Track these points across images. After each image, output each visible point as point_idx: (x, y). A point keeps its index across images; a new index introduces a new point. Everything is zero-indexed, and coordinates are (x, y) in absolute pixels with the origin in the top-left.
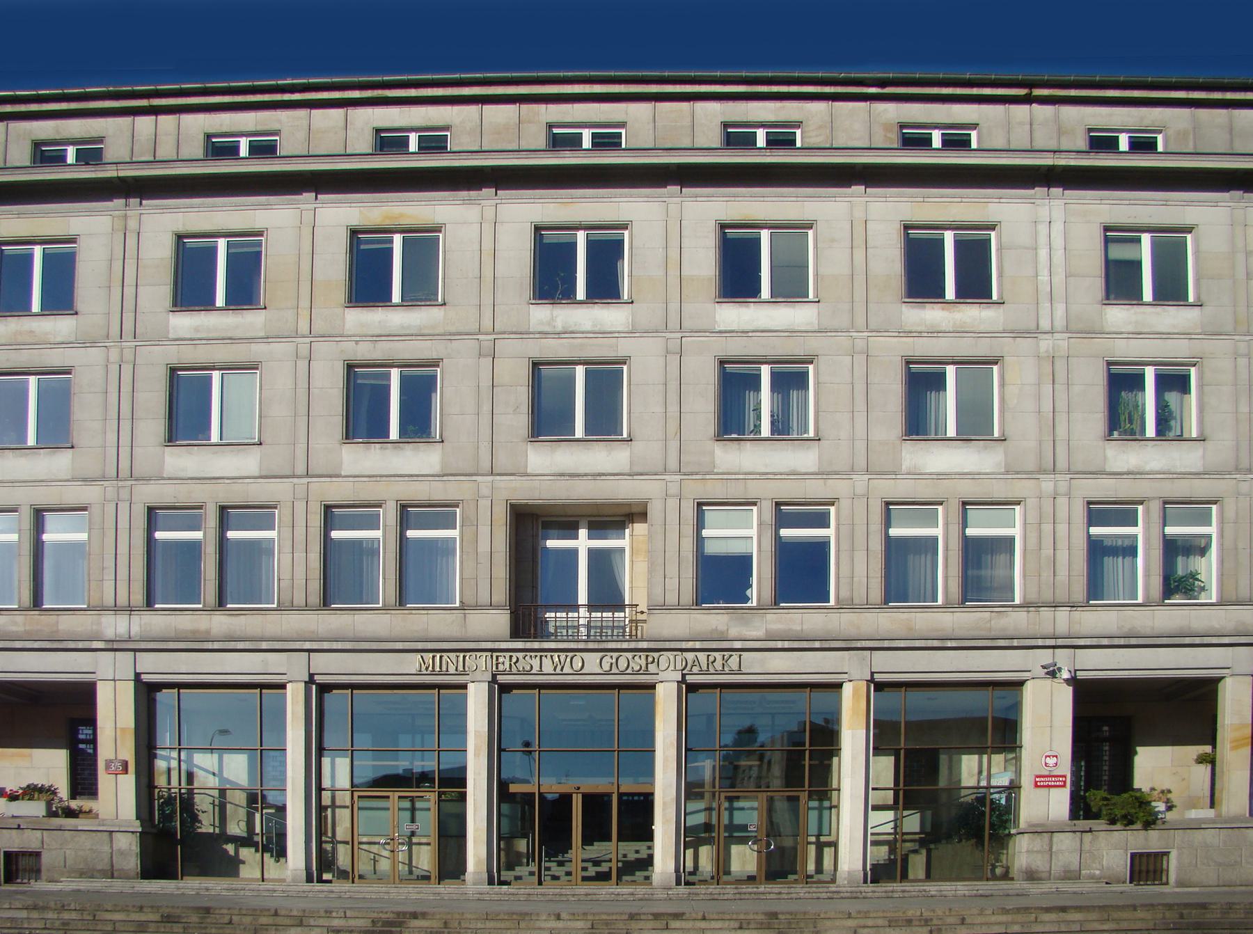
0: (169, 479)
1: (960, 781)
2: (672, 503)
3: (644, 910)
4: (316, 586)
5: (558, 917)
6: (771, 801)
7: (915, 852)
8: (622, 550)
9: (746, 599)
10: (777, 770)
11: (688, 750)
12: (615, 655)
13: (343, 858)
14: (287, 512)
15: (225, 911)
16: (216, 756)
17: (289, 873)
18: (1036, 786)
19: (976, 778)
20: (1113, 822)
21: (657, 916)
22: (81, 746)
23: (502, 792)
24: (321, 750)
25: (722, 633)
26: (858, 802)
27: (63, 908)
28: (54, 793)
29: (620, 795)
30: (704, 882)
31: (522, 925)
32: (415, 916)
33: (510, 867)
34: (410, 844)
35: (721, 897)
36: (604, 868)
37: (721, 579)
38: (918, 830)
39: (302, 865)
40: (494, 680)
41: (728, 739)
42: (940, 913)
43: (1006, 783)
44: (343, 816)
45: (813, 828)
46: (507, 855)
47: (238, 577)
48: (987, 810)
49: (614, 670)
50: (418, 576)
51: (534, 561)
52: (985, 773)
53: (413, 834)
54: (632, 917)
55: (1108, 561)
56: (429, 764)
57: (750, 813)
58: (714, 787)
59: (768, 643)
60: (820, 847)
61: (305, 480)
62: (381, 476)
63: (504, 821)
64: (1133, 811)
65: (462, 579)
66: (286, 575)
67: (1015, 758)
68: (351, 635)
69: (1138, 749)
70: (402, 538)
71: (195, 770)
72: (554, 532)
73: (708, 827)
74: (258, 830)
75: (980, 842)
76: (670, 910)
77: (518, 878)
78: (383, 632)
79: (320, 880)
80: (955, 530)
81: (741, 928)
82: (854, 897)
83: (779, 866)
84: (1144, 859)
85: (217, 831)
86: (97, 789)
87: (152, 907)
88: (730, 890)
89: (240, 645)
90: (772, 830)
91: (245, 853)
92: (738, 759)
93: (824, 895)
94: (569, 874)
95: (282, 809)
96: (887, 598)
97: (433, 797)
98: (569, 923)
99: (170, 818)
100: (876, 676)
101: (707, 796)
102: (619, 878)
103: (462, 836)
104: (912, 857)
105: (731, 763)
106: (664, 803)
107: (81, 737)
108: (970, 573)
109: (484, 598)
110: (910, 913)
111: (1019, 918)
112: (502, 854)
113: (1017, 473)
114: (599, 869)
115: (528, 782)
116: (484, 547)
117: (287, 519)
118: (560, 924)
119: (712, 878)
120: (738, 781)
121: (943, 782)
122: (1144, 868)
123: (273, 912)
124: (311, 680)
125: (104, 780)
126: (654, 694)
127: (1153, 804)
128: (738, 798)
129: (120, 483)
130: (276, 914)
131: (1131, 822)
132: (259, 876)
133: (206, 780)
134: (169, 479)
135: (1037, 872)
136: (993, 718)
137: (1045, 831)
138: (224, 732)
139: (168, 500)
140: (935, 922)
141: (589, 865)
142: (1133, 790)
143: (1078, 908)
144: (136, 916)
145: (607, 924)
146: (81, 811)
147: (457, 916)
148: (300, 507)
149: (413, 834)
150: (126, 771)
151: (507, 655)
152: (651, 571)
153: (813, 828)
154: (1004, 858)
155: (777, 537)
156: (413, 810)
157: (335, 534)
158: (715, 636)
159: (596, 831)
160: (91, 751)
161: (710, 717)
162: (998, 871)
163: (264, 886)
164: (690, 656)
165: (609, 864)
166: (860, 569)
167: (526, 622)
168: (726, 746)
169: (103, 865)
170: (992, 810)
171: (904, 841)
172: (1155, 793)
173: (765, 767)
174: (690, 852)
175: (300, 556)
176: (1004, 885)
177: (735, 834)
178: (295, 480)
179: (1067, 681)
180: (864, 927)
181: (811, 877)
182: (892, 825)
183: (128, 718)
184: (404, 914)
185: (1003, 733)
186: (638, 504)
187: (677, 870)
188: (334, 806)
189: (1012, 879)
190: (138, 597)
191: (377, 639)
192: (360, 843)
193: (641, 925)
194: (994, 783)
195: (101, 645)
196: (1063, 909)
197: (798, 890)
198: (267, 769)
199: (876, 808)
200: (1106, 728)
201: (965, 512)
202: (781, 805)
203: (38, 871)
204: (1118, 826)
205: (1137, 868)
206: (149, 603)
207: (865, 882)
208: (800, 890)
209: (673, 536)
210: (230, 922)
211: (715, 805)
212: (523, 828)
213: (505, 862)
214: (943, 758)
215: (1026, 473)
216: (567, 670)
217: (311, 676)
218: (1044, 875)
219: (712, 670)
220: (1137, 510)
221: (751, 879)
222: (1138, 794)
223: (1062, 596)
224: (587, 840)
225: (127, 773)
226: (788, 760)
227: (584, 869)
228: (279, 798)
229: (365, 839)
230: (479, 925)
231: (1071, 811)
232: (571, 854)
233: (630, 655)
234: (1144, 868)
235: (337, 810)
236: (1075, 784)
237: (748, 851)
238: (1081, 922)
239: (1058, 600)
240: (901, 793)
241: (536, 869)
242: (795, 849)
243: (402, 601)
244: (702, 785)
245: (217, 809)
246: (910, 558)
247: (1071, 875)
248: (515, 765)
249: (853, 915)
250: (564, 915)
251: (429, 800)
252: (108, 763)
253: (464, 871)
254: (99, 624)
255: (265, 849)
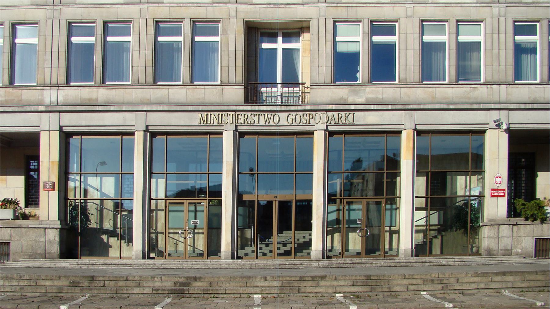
0: (79, 4)
1: (456, 192)
2: (322, 21)
3: (308, 274)
4: (150, 70)
5: (266, 279)
6: (368, 204)
7: (436, 237)
8: (298, 50)
9: (356, 79)
10: (371, 186)
11: (329, 173)
12: (295, 114)
13: (160, 245)
14: (137, 25)
15: (101, 278)
16: (99, 178)
17: (134, 253)
18: (492, 196)
19: (464, 190)
20: (527, 219)
21: (313, 278)
22: (32, 173)
23: (240, 201)
24: (151, 173)
25: (345, 100)
26: (409, 214)
27: (21, 278)
28: (18, 204)
29: (297, 201)
30: (336, 256)
31: (248, 285)
32: (195, 279)
33: (243, 248)
34: (194, 233)
35: (344, 266)
36: (288, 248)
37: (344, 66)
38: (437, 223)
39: (140, 248)
40: (236, 130)
41: (348, 166)
42: (447, 276)
43: (478, 194)
44: (161, 214)
45: (388, 223)
46: (241, 240)
47: (112, 65)
48: (469, 210)
49: (294, 124)
50: (200, 68)
51: (256, 56)
52: (468, 188)
53: (195, 227)
54: (302, 278)
55: (524, 56)
56: (203, 183)
57: (358, 213)
58: (341, 196)
59: (368, 106)
60: (392, 233)
61: (146, 6)
62: (183, 4)
63: (240, 218)
64: (536, 212)
65: (221, 67)
66: (135, 69)
67: (481, 178)
68: (166, 101)
69: (539, 173)
70: (193, 41)
71: (88, 188)
72: (265, 39)
73: (338, 221)
74: (119, 226)
75: (466, 232)
76: (319, 274)
77: (246, 254)
78: (182, 100)
79: (150, 258)
80: (453, 36)
81: (353, 285)
82: (407, 265)
83: (372, 247)
84: (541, 242)
85: (98, 227)
86: (39, 201)
87: (65, 276)
88: (348, 261)
89: (113, 108)
90: (369, 224)
91: (113, 241)
92: (352, 179)
93: (393, 265)
94: (271, 252)
95: (131, 212)
96: (422, 79)
97: (205, 203)
98: (271, 283)
99: (74, 219)
100: (417, 126)
101: (338, 201)
102: (295, 254)
103: (219, 228)
104: (434, 240)
105: (349, 181)
106: (317, 206)
107: (32, 167)
108: (460, 63)
109: (232, 80)
110: (433, 276)
111: (484, 279)
112: (239, 239)
113: (482, 3)
114: (286, 248)
115: (251, 193)
116: (232, 48)
117: (137, 30)
118: (266, 284)
119: (340, 254)
120: (353, 192)
121: (448, 194)
122: (541, 248)
123: (125, 278)
124: (147, 130)
125: (43, 195)
126: (313, 138)
127: (545, 208)
128: (352, 203)
129: (55, 7)
130: (127, 280)
131: (535, 220)
132: (119, 256)
133: (94, 194)
134: (79, 4)
135: (492, 250)
136: (472, 153)
137: (495, 224)
138: (103, 163)
139: (78, 18)
140: (445, 281)
141: (281, 246)
142: (536, 199)
143: (511, 273)
144: (57, 283)
145: (289, 283)
146: (30, 216)
147: (216, 279)
148: (143, 21)
149: (195, 227)
150: (53, 189)
151: (243, 113)
152: (312, 62)
153: (388, 223)
154: (477, 241)
155: (371, 41)
156: (196, 211)
157: (161, 39)
158: (342, 102)
159: (284, 226)
160: (36, 177)
161: (339, 151)
162: (474, 249)
163: (123, 262)
164: (330, 114)
165: (290, 245)
166: (410, 60)
167: (252, 95)
168: (347, 170)
169: (40, 251)
170: (471, 211)
171: (430, 230)
172: (546, 201)
173: (365, 182)
174: (329, 237)
175: (142, 52)
176: (476, 258)
177: (351, 226)
178: (141, 6)
179: (505, 130)
180: (412, 284)
181: (386, 253)
182: (425, 220)
183: (55, 156)
184: (190, 278)
185: (475, 163)
186: (305, 21)
187: (323, 249)
188: (157, 210)
189: (480, 255)
190: (62, 79)
191: (181, 104)
192: (169, 233)
193: (306, 283)
194: (472, 194)
195: (42, 109)
196: (504, 274)
197: (380, 261)
198: (124, 186)
199: (418, 209)
200: (523, 160)
201: (458, 25)
202: (373, 207)
203: (8, 255)
204: (529, 222)
205: (538, 248)
206: (68, 82)
207: (412, 256)
208: (382, 261)
209: (322, 41)
210: (104, 286)
211: (341, 207)
212: (249, 223)
213: (241, 243)
214: (449, 178)
215: (486, 3)
216: (272, 123)
217: (147, 127)
218: (495, 252)
219: (340, 123)
220: (536, 26)
221: (358, 254)
222: (538, 202)
223: (503, 79)
224: (280, 231)
225: (54, 190)
226: (376, 179)
227: (279, 249)
228: (130, 205)
229: (171, 231)
230: (227, 285)
231: (508, 212)
232: (272, 239)
233: (301, 114)
234: (541, 248)
235: (159, 212)
236: (509, 195)
237: (357, 236)
238: (512, 282)
239: (501, 80)
240: (429, 199)
241: (255, 249)
242: (379, 235)
243: (192, 80)
244: (335, 195)
245: (99, 212)
246: (433, 54)
247: (508, 253)
248: (246, 183)
249: (407, 277)
250: (269, 278)
251: (203, 205)
252: (45, 183)
253: (219, 251)
254: (42, 95)
255: (122, 238)
